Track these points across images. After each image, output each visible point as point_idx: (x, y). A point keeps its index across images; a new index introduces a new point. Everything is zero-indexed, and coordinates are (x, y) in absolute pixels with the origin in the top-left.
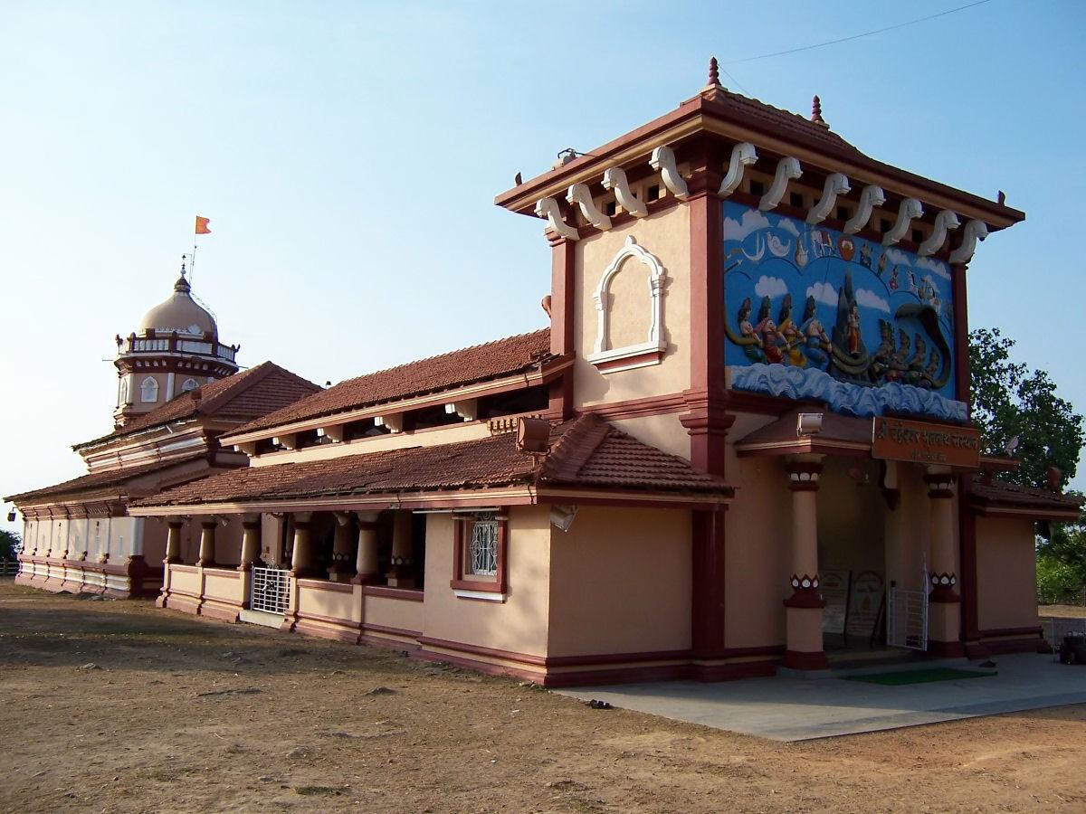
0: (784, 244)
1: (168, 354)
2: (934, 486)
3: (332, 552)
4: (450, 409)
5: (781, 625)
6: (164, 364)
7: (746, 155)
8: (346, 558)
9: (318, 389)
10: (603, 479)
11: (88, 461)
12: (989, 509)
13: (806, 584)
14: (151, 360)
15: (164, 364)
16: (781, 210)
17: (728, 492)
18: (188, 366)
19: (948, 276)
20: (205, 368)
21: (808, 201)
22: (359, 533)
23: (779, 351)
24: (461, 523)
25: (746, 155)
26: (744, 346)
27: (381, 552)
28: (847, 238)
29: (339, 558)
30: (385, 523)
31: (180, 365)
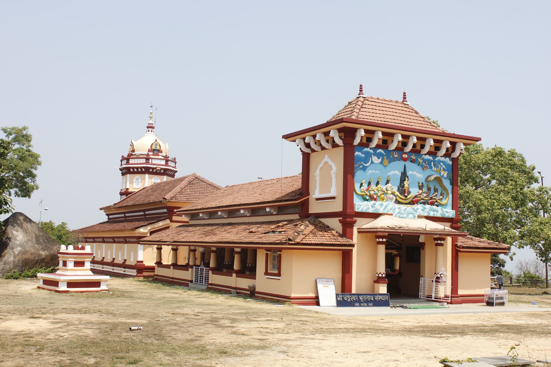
0: (379, 158)
1: (145, 165)
2: (436, 242)
3: (224, 261)
4: (268, 210)
5: (373, 288)
6: (143, 170)
7: (362, 133)
8: (230, 263)
9: (217, 188)
10: (308, 242)
11: (108, 215)
12: (462, 250)
13: (380, 275)
14: (137, 168)
15: (143, 170)
16: (378, 147)
17: (353, 246)
18: (155, 171)
19: (451, 163)
20: (162, 171)
21: (389, 142)
22: (234, 257)
23: (375, 196)
24: (267, 255)
25: (362, 133)
26: (362, 195)
27: (243, 262)
28: (405, 153)
29: (250, 265)
30: (244, 252)
31: (151, 170)
